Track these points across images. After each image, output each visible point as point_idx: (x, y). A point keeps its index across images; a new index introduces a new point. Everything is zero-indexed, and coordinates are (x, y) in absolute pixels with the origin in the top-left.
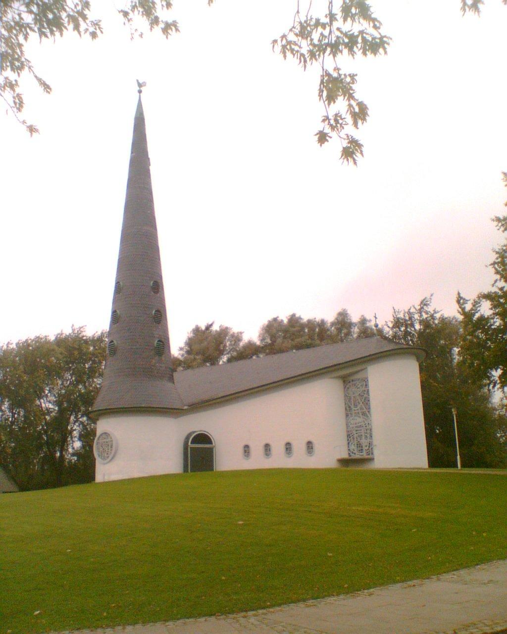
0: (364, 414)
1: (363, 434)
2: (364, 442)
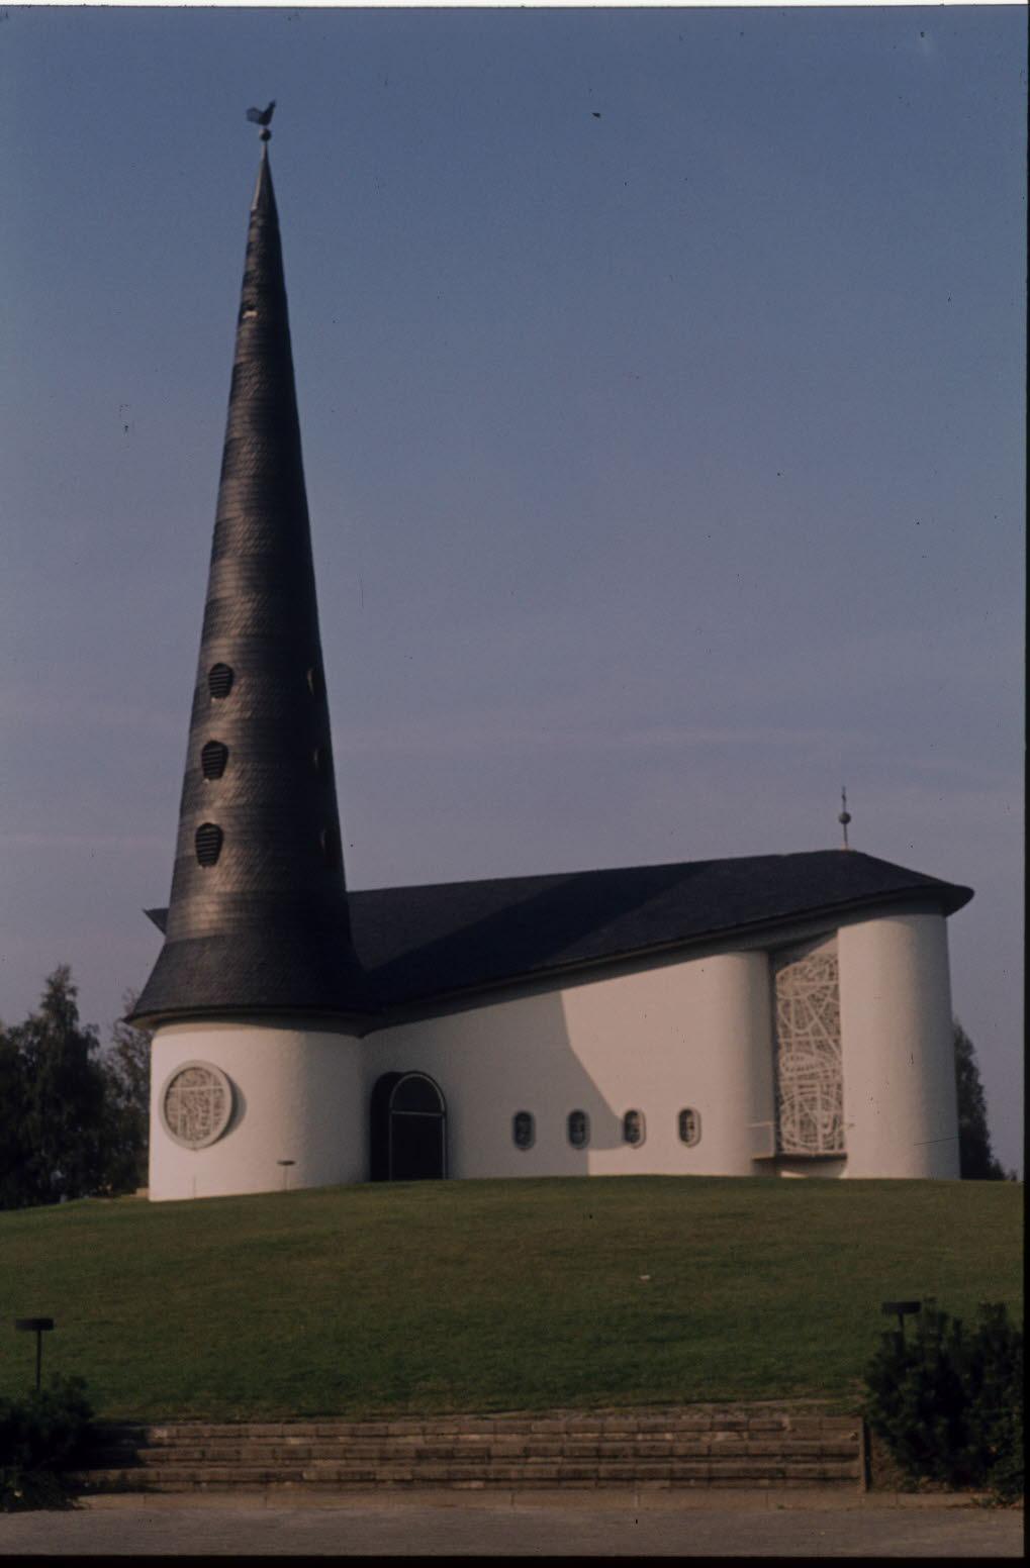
0: (821, 1046)
1: (818, 1095)
2: (821, 1115)
